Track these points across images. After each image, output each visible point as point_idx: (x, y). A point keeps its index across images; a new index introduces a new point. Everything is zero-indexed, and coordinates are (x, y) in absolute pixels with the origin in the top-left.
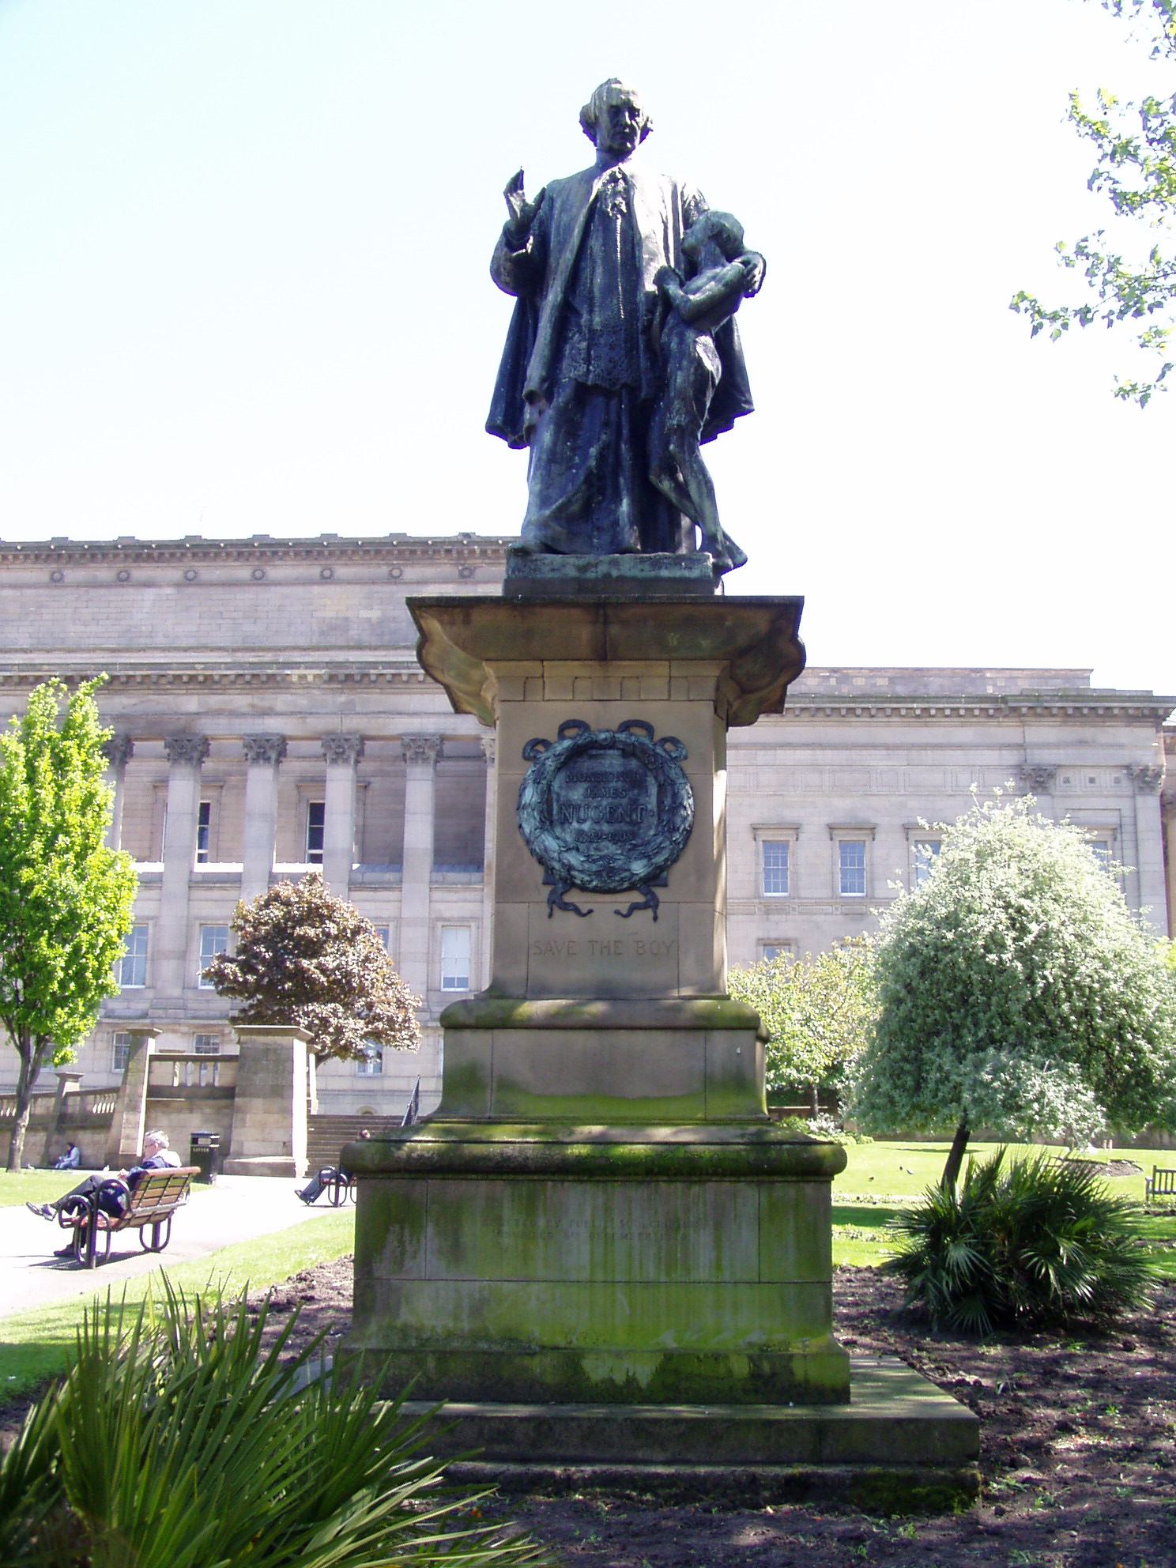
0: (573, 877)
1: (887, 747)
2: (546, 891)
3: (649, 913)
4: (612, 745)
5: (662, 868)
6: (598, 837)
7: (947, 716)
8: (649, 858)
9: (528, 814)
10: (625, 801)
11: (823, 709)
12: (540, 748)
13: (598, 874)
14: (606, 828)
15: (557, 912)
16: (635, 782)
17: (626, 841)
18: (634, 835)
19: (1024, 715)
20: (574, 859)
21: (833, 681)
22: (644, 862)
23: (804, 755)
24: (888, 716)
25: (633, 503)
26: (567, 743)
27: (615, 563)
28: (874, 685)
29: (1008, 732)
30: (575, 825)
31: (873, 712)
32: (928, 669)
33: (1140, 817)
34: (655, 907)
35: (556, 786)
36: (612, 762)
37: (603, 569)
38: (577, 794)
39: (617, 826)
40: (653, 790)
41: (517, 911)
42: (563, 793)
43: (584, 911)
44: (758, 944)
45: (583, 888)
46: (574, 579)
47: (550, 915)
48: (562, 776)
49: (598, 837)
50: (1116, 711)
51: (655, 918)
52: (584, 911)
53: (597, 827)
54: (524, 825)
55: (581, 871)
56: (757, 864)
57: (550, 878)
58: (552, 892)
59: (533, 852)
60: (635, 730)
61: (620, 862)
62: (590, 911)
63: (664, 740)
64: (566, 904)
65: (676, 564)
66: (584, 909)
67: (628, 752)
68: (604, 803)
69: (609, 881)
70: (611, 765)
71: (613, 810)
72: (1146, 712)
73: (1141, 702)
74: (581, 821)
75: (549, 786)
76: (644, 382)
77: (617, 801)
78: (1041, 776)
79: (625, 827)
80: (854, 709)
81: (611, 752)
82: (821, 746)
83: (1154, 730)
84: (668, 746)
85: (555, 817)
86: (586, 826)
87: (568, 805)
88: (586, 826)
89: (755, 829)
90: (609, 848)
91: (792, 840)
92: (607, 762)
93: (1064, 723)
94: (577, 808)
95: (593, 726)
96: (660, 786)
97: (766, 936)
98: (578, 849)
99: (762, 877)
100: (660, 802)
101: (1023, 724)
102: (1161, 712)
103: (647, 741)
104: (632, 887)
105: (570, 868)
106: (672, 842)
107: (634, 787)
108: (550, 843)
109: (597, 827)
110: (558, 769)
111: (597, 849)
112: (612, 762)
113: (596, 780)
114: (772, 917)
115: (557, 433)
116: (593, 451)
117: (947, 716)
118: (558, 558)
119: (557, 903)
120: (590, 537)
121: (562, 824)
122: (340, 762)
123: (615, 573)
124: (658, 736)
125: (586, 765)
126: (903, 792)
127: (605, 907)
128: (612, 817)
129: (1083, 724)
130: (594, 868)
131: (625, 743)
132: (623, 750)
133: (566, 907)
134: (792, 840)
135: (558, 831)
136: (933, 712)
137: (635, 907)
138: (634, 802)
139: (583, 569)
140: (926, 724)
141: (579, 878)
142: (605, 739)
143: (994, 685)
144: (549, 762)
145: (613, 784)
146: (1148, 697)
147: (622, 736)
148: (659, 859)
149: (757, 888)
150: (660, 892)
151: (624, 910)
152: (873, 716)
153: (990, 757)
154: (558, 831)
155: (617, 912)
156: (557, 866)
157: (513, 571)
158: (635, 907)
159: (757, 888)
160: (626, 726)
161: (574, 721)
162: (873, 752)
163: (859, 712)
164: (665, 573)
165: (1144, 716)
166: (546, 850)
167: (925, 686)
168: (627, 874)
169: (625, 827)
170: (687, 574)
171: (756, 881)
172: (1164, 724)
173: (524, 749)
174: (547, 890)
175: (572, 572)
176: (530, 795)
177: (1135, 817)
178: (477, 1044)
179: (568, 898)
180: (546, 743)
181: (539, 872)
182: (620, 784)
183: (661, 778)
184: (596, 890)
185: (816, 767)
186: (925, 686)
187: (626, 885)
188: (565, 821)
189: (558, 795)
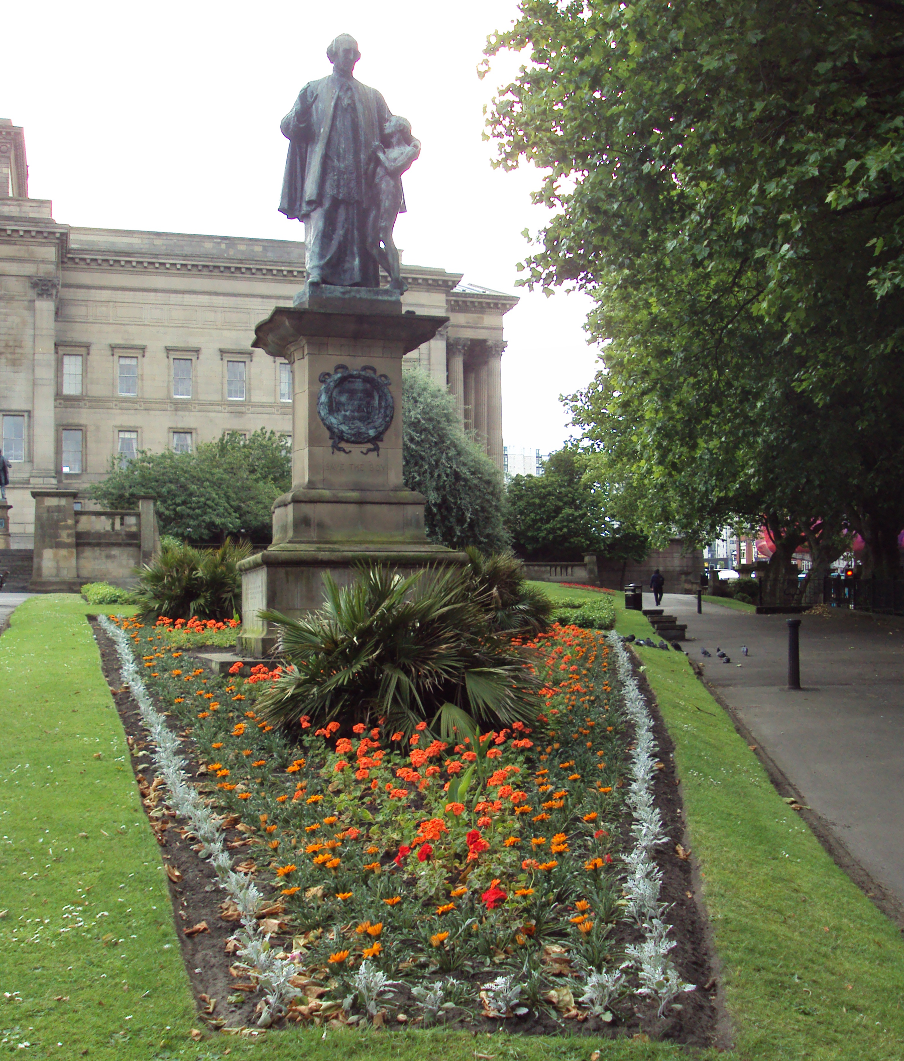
1: (263, 297)
2: (331, 442)
3: (375, 453)
4: (359, 377)
6: (354, 418)
11: (219, 267)
13: (354, 435)
14: (356, 414)
16: (369, 395)
18: (368, 418)
20: (344, 428)
21: (223, 246)
23: (204, 299)
24: (264, 274)
25: (360, 261)
26: (339, 375)
27: (359, 292)
28: (253, 251)
30: (343, 412)
31: (254, 271)
33: (432, 355)
35: (334, 394)
36: (358, 385)
37: (353, 294)
38: (343, 399)
40: (377, 398)
41: (318, 450)
44: (169, 432)
45: (347, 441)
46: (340, 298)
49: (354, 418)
50: (420, 281)
56: (169, 375)
58: (334, 442)
59: (325, 424)
60: (369, 371)
63: (381, 376)
66: (347, 450)
67: (366, 380)
69: (358, 439)
71: (359, 407)
72: (440, 283)
74: (345, 411)
80: (240, 268)
82: (216, 294)
84: (383, 378)
88: (348, 413)
89: (168, 350)
90: (358, 423)
91: (194, 359)
94: (344, 405)
95: (350, 368)
97: (174, 426)
99: (172, 384)
100: (380, 403)
102: (450, 283)
103: (373, 376)
104: (369, 441)
105: (342, 432)
108: (334, 421)
110: (335, 387)
112: (358, 385)
113: (352, 393)
114: (180, 413)
118: (332, 287)
119: (336, 447)
122: (45, 296)
123: (358, 296)
124: (378, 374)
125: (347, 385)
127: (356, 450)
128: (359, 409)
130: (353, 432)
133: (340, 449)
134: (194, 359)
135: (335, 415)
136: (295, 273)
137: (369, 450)
139: (344, 293)
140: (291, 282)
141: (346, 436)
146: (442, 273)
147: (363, 373)
148: (381, 429)
149: (169, 391)
150: (380, 444)
151: (365, 451)
152: (253, 274)
156: (336, 430)
158: (369, 450)
159: (169, 391)
160: (365, 368)
162: (252, 299)
163: (243, 270)
164: (380, 298)
165: (439, 286)
167: (288, 253)
169: (365, 414)
170: (390, 298)
171: (168, 387)
174: (332, 441)
175: (339, 295)
176: (324, 398)
177: (429, 354)
178: (307, 509)
179: (340, 445)
180: (328, 374)
181: (327, 434)
184: (353, 442)
185: (212, 307)
186: (288, 253)
188: (338, 410)
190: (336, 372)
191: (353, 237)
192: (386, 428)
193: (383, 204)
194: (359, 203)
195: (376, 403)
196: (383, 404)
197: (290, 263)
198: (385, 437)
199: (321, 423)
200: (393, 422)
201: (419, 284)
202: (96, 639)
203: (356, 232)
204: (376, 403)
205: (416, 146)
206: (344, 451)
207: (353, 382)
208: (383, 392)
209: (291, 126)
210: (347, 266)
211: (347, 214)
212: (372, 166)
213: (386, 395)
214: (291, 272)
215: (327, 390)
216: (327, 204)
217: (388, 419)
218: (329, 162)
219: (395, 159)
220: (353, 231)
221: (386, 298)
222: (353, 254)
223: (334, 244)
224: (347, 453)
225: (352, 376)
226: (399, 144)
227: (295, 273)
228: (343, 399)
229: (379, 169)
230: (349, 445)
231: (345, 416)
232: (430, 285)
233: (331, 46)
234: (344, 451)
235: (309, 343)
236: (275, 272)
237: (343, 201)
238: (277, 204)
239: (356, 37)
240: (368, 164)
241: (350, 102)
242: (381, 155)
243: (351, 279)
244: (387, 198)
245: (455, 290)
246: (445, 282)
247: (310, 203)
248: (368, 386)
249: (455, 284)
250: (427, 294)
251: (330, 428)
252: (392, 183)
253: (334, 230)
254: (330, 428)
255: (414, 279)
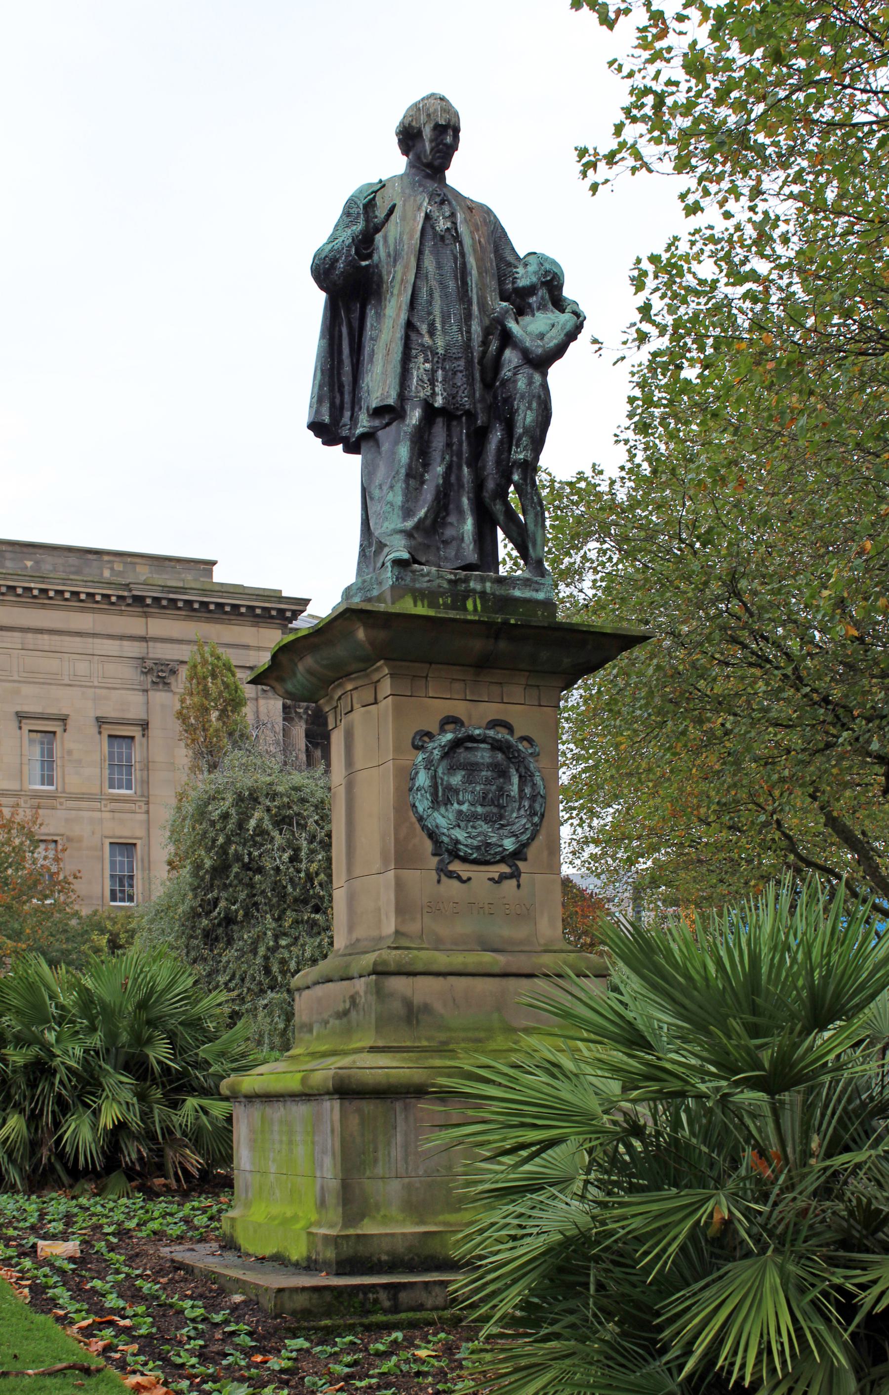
0: (459, 850)
3: (514, 882)
5: (525, 845)
6: (474, 817)
7: (66, 600)
8: (516, 836)
9: (422, 795)
10: (494, 787)
12: (426, 739)
13: (478, 848)
14: (479, 809)
15: (444, 879)
17: (495, 822)
18: (501, 817)
19: (148, 606)
20: (459, 834)
22: (513, 839)
26: (449, 736)
29: (133, 624)
30: (456, 806)
32: (98, 553)
34: (519, 876)
36: (483, 755)
38: (456, 780)
39: (488, 809)
40: (515, 780)
41: (412, 876)
42: (446, 778)
43: (465, 878)
45: (465, 860)
47: (439, 881)
48: (444, 763)
49: (474, 817)
50: (243, 610)
51: (519, 886)
52: (465, 878)
53: (473, 809)
54: (417, 804)
55: (466, 846)
57: (438, 847)
59: (424, 827)
61: (495, 839)
62: (469, 879)
63: (524, 739)
64: (451, 872)
65: (526, 586)
67: (497, 746)
68: (478, 789)
70: (482, 757)
73: (293, 604)
74: (460, 803)
75: (435, 771)
76: (479, 411)
77: (488, 787)
78: (162, 671)
79: (495, 810)
81: (482, 746)
83: (280, 632)
84: (525, 743)
85: (440, 799)
86: (465, 808)
87: (449, 788)
88: (465, 808)
90: (485, 827)
92: (479, 754)
93: (188, 618)
94: (456, 792)
96: (520, 777)
98: (459, 826)
100: (521, 790)
101: (146, 615)
102: (288, 614)
103: (508, 737)
104: (502, 860)
105: (457, 842)
106: (533, 824)
107: (500, 777)
109: (473, 809)
110: (442, 758)
111: (474, 827)
112: (483, 755)
113: (471, 769)
115: (412, 450)
116: (440, 470)
117: (66, 600)
119: (443, 871)
120: (438, 549)
121: (446, 805)
124: (518, 733)
125: (462, 755)
126: (16, 678)
127: (481, 875)
128: (484, 800)
129: (208, 620)
131: (494, 739)
132: (491, 744)
133: (451, 875)
136: (51, 594)
137: (503, 877)
138: (501, 789)
140: (44, 606)
141: (463, 850)
142: (479, 735)
143: (112, 569)
144: (436, 752)
145: (484, 773)
146: (276, 596)
147: (491, 733)
148: (524, 838)
151: (496, 876)
153: (111, 647)
154: (443, 810)
155: (490, 879)
156: (446, 839)
157: (397, 579)
158: (503, 877)
160: (494, 724)
161: (448, 717)
165: (272, 617)
166: (437, 827)
168: (500, 849)
172: (290, 626)
173: (414, 738)
176: (423, 779)
179: (451, 868)
180: (429, 735)
181: (429, 845)
182: (489, 773)
183: (522, 770)
184: (475, 862)
187: (498, 858)
188: (447, 802)
189: (442, 779)
190: (442, 730)
191: (459, 478)
192: (532, 838)
193: (519, 418)
194: (470, 415)
195: (514, 789)
196: (528, 791)
197: (43, 579)
198: (531, 852)
199: (417, 826)
200: (545, 823)
201: (242, 614)
202: (328, 1274)
203: (466, 470)
204: (514, 789)
205: (577, 314)
206: (459, 878)
207: (477, 749)
208: (527, 769)
209: (341, 265)
210: (449, 532)
211: (449, 436)
212: (494, 347)
213: (532, 775)
214: (44, 591)
215: (429, 764)
216: (415, 416)
217: (536, 819)
218: (413, 336)
219: (541, 336)
220: (460, 468)
221: (528, 594)
222: (461, 512)
223: (428, 493)
224: (464, 882)
225: (471, 739)
226: (542, 307)
227: (51, 594)
228: (456, 780)
229: (508, 353)
230: (467, 866)
231: (460, 812)
232: (258, 616)
233: (402, 123)
234: (459, 878)
235: (392, 675)
236: (20, 591)
237: (442, 411)
238: (304, 415)
239: (457, 103)
240: (485, 343)
241: (449, 225)
242: (512, 325)
243: (457, 557)
244: (529, 408)
245: (295, 624)
246: (281, 612)
247: (379, 412)
248: (500, 756)
249: (296, 614)
250: (254, 629)
251: (432, 835)
252: (537, 377)
253: (426, 465)
254: (432, 835)
255: (218, 605)
